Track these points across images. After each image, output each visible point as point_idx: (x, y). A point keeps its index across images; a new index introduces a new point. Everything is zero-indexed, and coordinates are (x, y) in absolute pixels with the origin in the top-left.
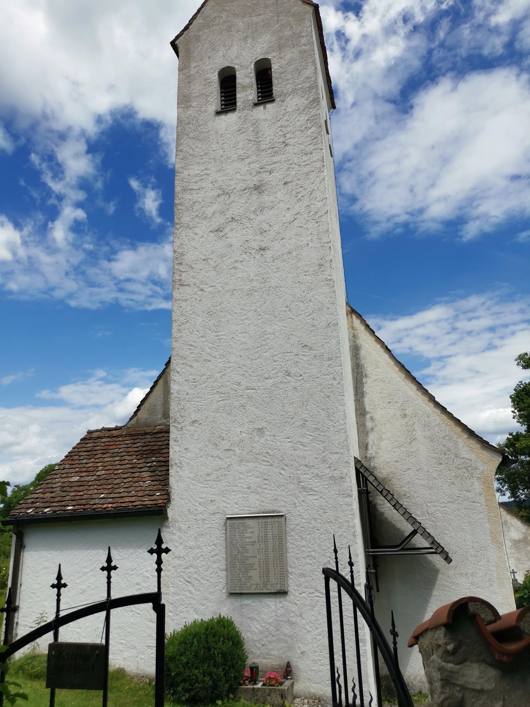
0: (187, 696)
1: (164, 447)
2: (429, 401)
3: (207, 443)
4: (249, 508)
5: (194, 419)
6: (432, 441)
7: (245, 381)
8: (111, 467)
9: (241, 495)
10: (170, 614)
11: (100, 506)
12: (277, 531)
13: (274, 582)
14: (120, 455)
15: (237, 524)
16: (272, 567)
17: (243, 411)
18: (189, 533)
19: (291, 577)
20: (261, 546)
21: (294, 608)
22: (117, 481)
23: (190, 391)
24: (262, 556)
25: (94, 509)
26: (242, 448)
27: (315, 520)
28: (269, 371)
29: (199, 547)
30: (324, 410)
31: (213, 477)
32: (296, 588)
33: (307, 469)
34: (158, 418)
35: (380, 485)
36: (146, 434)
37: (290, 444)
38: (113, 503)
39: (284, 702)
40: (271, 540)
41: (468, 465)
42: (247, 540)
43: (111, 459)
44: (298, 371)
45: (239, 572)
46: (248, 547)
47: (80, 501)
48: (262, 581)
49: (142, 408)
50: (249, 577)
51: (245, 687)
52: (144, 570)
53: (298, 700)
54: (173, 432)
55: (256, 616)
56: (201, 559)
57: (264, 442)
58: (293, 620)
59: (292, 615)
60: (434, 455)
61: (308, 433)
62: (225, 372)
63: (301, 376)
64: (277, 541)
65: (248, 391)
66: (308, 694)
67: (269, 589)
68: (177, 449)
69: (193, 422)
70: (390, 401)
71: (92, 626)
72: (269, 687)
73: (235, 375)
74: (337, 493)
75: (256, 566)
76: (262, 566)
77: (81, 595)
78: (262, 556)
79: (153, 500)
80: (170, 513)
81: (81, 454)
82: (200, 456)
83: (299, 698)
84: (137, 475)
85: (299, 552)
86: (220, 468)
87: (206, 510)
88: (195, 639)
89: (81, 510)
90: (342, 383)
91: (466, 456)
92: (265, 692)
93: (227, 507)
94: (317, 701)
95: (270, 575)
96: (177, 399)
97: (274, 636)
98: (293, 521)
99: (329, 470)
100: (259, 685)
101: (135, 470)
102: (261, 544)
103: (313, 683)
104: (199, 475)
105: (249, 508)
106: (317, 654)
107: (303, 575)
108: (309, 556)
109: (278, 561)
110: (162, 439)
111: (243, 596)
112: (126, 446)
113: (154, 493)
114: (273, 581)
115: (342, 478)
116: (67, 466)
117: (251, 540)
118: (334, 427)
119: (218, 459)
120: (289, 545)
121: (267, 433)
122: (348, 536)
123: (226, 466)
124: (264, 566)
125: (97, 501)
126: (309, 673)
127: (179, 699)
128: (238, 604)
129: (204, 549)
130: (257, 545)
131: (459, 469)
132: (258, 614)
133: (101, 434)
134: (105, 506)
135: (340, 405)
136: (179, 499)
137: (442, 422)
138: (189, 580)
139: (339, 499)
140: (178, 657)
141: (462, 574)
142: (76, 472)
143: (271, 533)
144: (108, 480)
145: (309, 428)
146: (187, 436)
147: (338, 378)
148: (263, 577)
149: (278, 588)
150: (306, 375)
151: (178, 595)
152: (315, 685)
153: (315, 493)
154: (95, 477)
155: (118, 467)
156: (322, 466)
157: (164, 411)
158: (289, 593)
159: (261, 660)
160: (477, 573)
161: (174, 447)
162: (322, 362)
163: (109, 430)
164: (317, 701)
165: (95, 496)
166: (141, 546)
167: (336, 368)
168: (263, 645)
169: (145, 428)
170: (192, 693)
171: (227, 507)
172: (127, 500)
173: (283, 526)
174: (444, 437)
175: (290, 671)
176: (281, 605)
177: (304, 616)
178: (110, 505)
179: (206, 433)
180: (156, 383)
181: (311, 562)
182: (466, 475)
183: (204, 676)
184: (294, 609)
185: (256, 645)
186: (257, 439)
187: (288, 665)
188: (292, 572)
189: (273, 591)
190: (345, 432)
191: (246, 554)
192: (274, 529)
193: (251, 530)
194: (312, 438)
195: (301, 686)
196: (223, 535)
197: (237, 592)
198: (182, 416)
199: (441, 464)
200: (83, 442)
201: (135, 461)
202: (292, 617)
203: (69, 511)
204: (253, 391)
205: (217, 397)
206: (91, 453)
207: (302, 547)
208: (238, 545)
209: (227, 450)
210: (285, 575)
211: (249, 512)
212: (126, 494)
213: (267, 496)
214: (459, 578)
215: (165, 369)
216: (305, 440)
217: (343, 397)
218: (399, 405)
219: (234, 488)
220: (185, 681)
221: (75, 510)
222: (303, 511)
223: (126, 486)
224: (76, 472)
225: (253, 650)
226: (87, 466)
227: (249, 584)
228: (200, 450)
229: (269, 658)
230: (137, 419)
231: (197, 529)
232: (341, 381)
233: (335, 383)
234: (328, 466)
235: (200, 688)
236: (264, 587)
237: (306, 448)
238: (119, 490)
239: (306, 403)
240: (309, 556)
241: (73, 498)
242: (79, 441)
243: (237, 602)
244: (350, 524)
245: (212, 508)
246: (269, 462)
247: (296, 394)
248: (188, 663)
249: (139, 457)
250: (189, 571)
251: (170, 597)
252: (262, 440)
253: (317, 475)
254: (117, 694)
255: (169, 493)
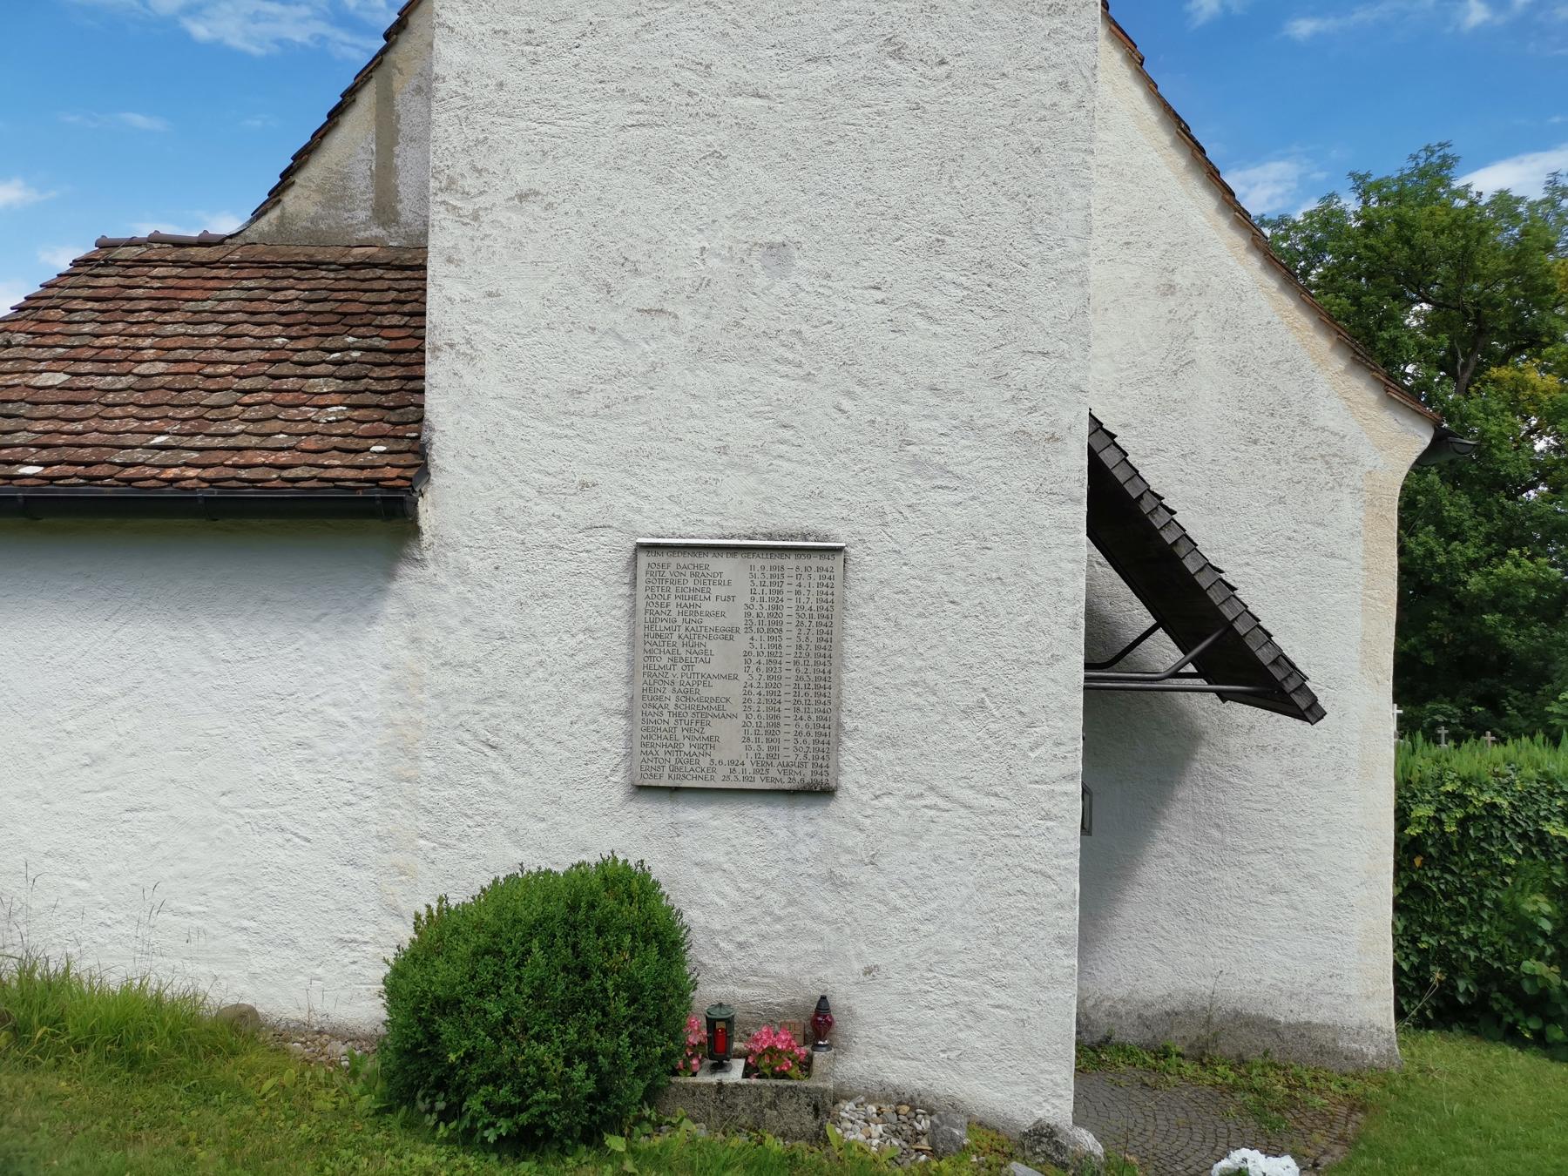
0: (504, 1126)
1: (384, 308)
2: (1249, 250)
3: (574, 280)
5: (525, 188)
6: (1239, 372)
7: (728, 60)
8: (190, 354)
9: (692, 474)
10: (422, 842)
11: (149, 472)
12: (813, 599)
13: (792, 759)
14: (224, 318)
15: (673, 568)
16: (791, 714)
17: (716, 173)
18: (498, 586)
19: (850, 744)
20: (757, 644)
21: (854, 839)
22: (214, 399)
23: (511, 78)
24: (756, 676)
25: (129, 481)
26: (704, 310)
27: (948, 569)
28: (823, 31)
29: (530, 636)
30: (1013, 197)
31: (590, 403)
32: (863, 779)
33: (933, 401)
34: (360, 226)
35: (1137, 479)
36: (317, 265)
37: (881, 309)
38: (204, 467)
39: (821, 1126)
40: (792, 627)
41: (1334, 450)
42: (709, 622)
43: (190, 330)
44: (937, 44)
45: (672, 720)
46: (711, 645)
47: (71, 451)
48: (751, 754)
49: (300, 178)
50: (709, 738)
51: (691, 1079)
52: (327, 698)
53: (850, 1106)
54: (442, 228)
55: (722, 859)
56: (540, 673)
57: (787, 295)
58: (848, 874)
59: (844, 859)
60: (1241, 414)
61: (949, 276)
62: (651, 17)
63: (942, 62)
64: (814, 630)
65: (740, 100)
66: (878, 1088)
67: (774, 780)
68: (456, 289)
69: (522, 197)
70: (1132, 239)
71: (132, 872)
72: (774, 1082)
73: (692, 34)
74: (1033, 488)
75: (736, 707)
76: (755, 707)
77: (87, 771)
78: (756, 676)
79: (362, 468)
80: (429, 513)
81: (75, 304)
82: (543, 323)
83: (849, 1098)
84: (289, 384)
85: (882, 669)
86: (620, 374)
87: (563, 514)
88: (535, 941)
89: (74, 481)
90: (1089, 106)
91: (1331, 424)
92: (760, 1097)
93: (639, 511)
94: (905, 1109)
95: (782, 736)
96: (458, 102)
97: (779, 919)
98: (872, 570)
99: (1011, 408)
100: (735, 1073)
101: (284, 369)
102: (756, 636)
103: (895, 1057)
104: (540, 391)
105: (717, 519)
106: (915, 975)
107: (892, 742)
108: (915, 684)
109: (812, 693)
110: (376, 285)
112: (244, 295)
113: (362, 444)
115: (1053, 438)
116: (20, 338)
118: (1044, 261)
119: (610, 342)
120: (850, 646)
121: (800, 263)
122: (1053, 627)
123: (641, 369)
124: (763, 707)
125: (139, 455)
126: (885, 1028)
127: (470, 1133)
128: (667, 819)
129: (551, 643)
130: (742, 641)
131: (1304, 460)
132: (728, 853)
133: (152, 254)
134: (171, 473)
135: (1074, 185)
136: (459, 470)
137: (1277, 319)
138: (493, 740)
139: (1038, 507)
140: (470, 1000)
141: (1263, 748)
142: (56, 359)
143: (793, 604)
144: (180, 391)
145: (955, 258)
146: (498, 247)
147: (1078, 85)
148: (757, 740)
149: (807, 776)
150: (963, 61)
151: (452, 785)
152: (902, 1063)
153: (956, 483)
154: (131, 379)
155: (217, 355)
156: (989, 393)
157: (378, 198)
158: (839, 794)
159: (731, 988)
160: (1307, 747)
161: (447, 283)
162: (1025, 19)
163: (180, 244)
164: (905, 1109)
165: (130, 439)
166: (317, 620)
167: (1075, 47)
168: (741, 946)
169: (312, 250)
170: (523, 1118)
171: (639, 511)
172: (260, 460)
173: (837, 582)
174: (1278, 363)
175: (830, 1024)
176: (810, 829)
177: (883, 862)
178: (191, 473)
179: (570, 241)
180: (349, 97)
181: (920, 701)
182: (1323, 477)
183: (568, 1062)
184: (850, 843)
185: (717, 945)
186: (761, 281)
187: (823, 1005)
188: (856, 729)
189: (786, 786)
190: (1081, 284)
191: (700, 668)
192: (804, 591)
194: (961, 293)
195: (856, 1065)
196: (620, 603)
198: (480, 171)
199: (1255, 442)
200: (80, 270)
201: (280, 340)
202: (842, 866)
203: (28, 482)
204: (759, 102)
205: (619, 111)
206: (111, 306)
207: (894, 653)
208: (675, 637)
209: (649, 311)
210: (833, 739)
211: (718, 531)
212: (255, 441)
213: (787, 481)
214: (1254, 757)
215: (384, 51)
216: (937, 301)
217: (1089, 158)
218: (1155, 254)
219: (668, 448)
220: (495, 1079)
221: (51, 479)
222: (907, 539)
223: (251, 413)
224: (56, 359)
225: (705, 959)
226: (97, 342)
227: (705, 762)
228: (548, 302)
229: (758, 985)
230: (282, 218)
231: (527, 576)
232: (1088, 96)
233: (1066, 102)
234: (1008, 395)
235: (555, 1102)
237: (939, 330)
238: (224, 427)
239: (950, 168)
240: (915, 684)
241: (45, 439)
242: (65, 267)
243: (659, 814)
244: (1065, 590)
245: (582, 509)
246: (799, 366)
247: (920, 129)
248: (510, 1022)
249: (294, 331)
250: (495, 710)
251: (424, 791)
252: (782, 288)
253: (970, 424)
254: (233, 1114)
255: (423, 446)
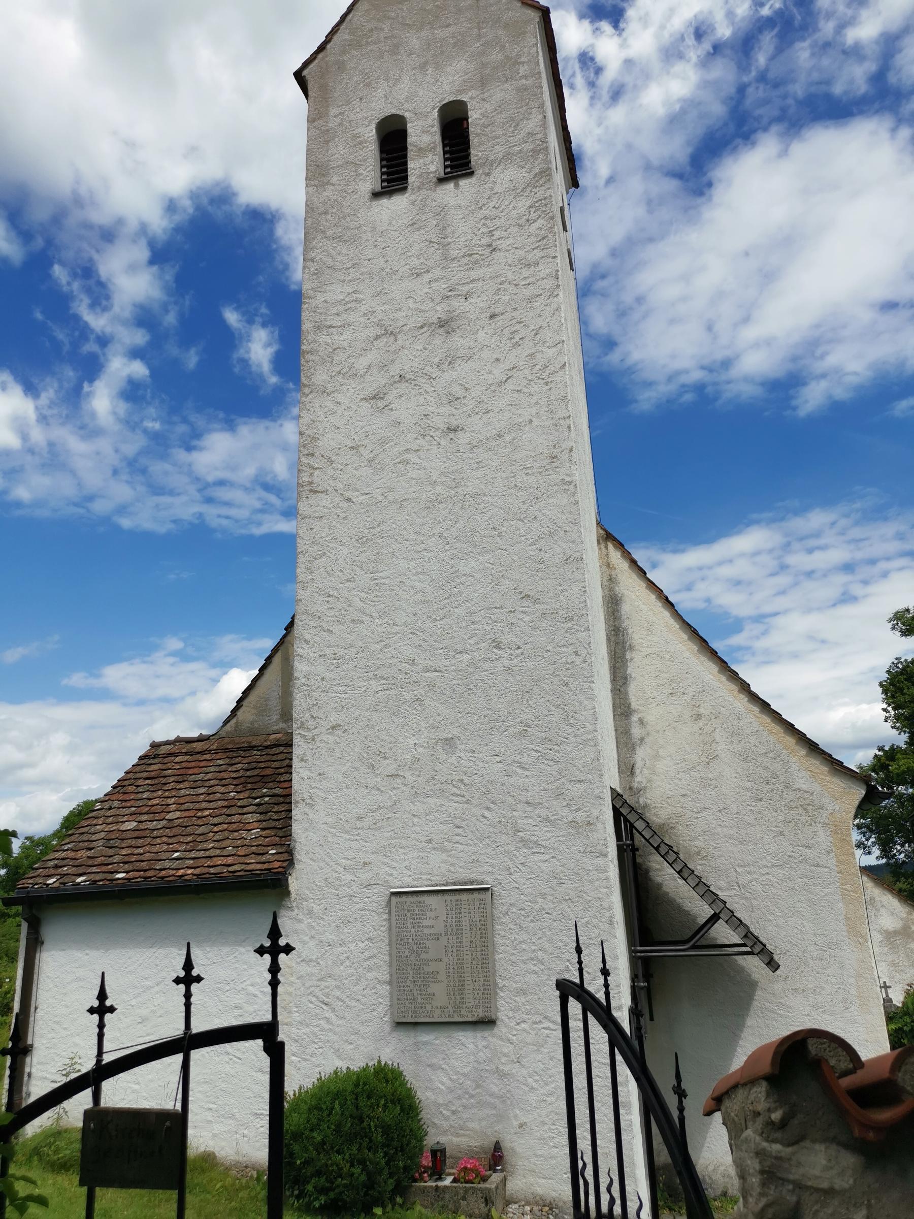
0: (323, 1199)
1: (282, 770)
2: (739, 691)
3: (357, 764)
4: (429, 877)
5: (334, 723)
6: (745, 760)
7: (422, 657)
8: (191, 806)
9: (416, 854)
10: (293, 1058)
11: (172, 872)
12: (477, 916)
13: (472, 1004)
14: (207, 784)
15: (408, 904)
16: (470, 978)
17: (419, 708)
18: (326, 918)
19: (502, 994)
20: (451, 942)
21: (507, 1049)
22: (201, 830)
23: (328, 675)
24: (451, 958)
25: (163, 878)
26: (417, 773)
27: (543, 896)
28: (463, 639)
29: (343, 944)
30: (558, 706)
31: (367, 823)
32: (510, 1014)
33: (529, 809)
34: (273, 720)
35: (655, 837)
36: (252, 748)
37: (500, 765)
38: (195, 868)
39: (489, 1211)
40: (467, 931)
41: (807, 802)
42: (426, 931)
43: (192, 792)
44: (514, 639)
45: (412, 986)
46: (428, 943)
47: (138, 864)
48: (452, 1002)
49: (245, 703)
50: (430, 994)
51: (422, 1184)
52: (248, 982)
53: (514, 1206)
54: (299, 746)
55: (441, 1062)
56: (347, 963)
57: (455, 762)
58: (506, 1068)
59: (503, 1060)
60: (749, 784)
61: (531, 747)
62: (387, 641)
63: (519, 648)
64: (478, 932)
65: (428, 674)
66: (532, 1197)
67: (464, 1016)
68: (305, 773)
69: (333, 728)
70: (673, 691)
71: (159, 1079)
72: (464, 1185)
73: (405, 647)
74: (582, 850)
75: (442, 976)
76: (452, 976)
77: (140, 1025)
78: (451, 958)
79: (264, 863)
80: (293, 884)
81: (140, 782)
82: (344, 785)
83: (515, 1203)
84: (235, 818)
85: (515, 952)
86: (380, 808)
87: (356, 879)
88: (337, 1102)
89: (139, 880)
90: (589, 661)
91: (804, 787)
92: (457, 1194)
93: (391, 875)
94: (547, 1208)
95: (466, 991)
96: (305, 688)
97: (472, 1096)
98: (505, 898)
99: (567, 810)
100: (447, 1181)
101: (233, 810)
102: (450, 937)
103: (539, 1177)
104: (344, 819)
105: (429, 877)
106: (546, 1127)
107: (522, 992)
108: (532, 959)
109: (479, 967)
110: (280, 757)
111: (420, 1028)
112: (217, 769)
113: (266, 849)
114: (470, 1001)
115: (589, 824)
116: (116, 804)
117: (432, 931)
118: (575, 736)
119: (375, 792)
120: (498, 940)
121: (460, 747)
122: (600, 924)
123: (389, 804)
124: (456, 976)
125: (167, 864)
126: (533, 1160)
127: (309, 1205)
128: (411, 1041)
129: (352, 946)
130: (443, 940)
131: (791, 808)
132: (444, 1059)
133: (175, 749)
134: (181, 872)
135: (586, 698)
136: (308, 861)
137: (762, 728)
138: (326, 1000)
139: (585, 860)
140: (307, 1133)
141: (796, 990)
142: (131, 815)
143: (467, 919)
144: (186, 827)
145: (533, 738)
146: (323, 752)
147: (583, 652)
148: (454, 994)
149: (479, 1014)
150: (528, 647)
151: (307, 1026)
152: (544, 1181)
153: (543, 850)
154: (164, 822)
155: (204, 805)
156: (555, 803)
157: (282, 708)
158: (498, 1023)
159: (450, 1137)
160: (823, 988)
161: (301, 770)
162: (555, 625)
163: (189, 741)
164: (547, 1208)
165: (163, 856)
166: (244, 941)
167: (580, 635)
168: (454, 1112)
169: (250, 739)
170: (332, 1195)
171: (391, 875)
172: (219, 862)
173: (488, 906)
174: (766, 753)
175: (501, 1157)
176: (484, 1043)
177: (524, 1061)
178: (189, 871)
179: (355, 746)
180: (269, 660)
181: (536, 968)
182: (804, 818)
183: (352, 1165)
184: (506, 1051)
185: (441, 1112)
186: (443, 757)
187: (497, 1147)
188: (504, 986)
189: (470, 1019)
190: (595, 745)
191: (424, 956)
192: (472, 912)
193: (432, 914)
194: (537, 755)
195: (520, 1183)
196: (384, 923)
197: (408, 1021)
198: (314, 718)
199: (761, 800)
200: (143, 762)
201: (232, 794)
202: (503, 1064)
203: (119, 882)
204: (437, 674)
205: (374, 685)
206: (157, 781)
207: (521, 942)
208: (411, 940)
209: (392, 776)
210: (492, 992)
211: (429, 883)
212: (218, 852)
213: (461, 854)
214: (791, 997)
215: (285, 636)
216: (526, 759)
217: (592, 685)
218: (687, 698)
219: (404, 842)
220: (318, 1173)
221: (129, 880)
222: (522, 881)
223: (217, 837)
224: (131, 815)
225: (436, 1121)
226: (150, 803)
227: (429, 1007)
228: (346, 775)
229: (464, 1135)
230: (237, 722)
231: (340, 912)
232: (588, 656)
233: (578, 660)
234: (565, 804)
235: (345, 1186)
236: (455, 1012)
237: (528, 773)
238: (205, 846)
239: (527, 695)
240: (532, 959)
241: (126, 859)
242: (135, 761)
243: (408, 1038)
244: (604, 904)
245: (365, 876)
246: (463, 796)
247: (511, 679)
248: (325, 1144)
249: (240, 788)
250: (327, 984)
251: (294, 1030)
252: (453, 759)
253: (547, 819)
254: (202, 1197)
255: (291, 850)
